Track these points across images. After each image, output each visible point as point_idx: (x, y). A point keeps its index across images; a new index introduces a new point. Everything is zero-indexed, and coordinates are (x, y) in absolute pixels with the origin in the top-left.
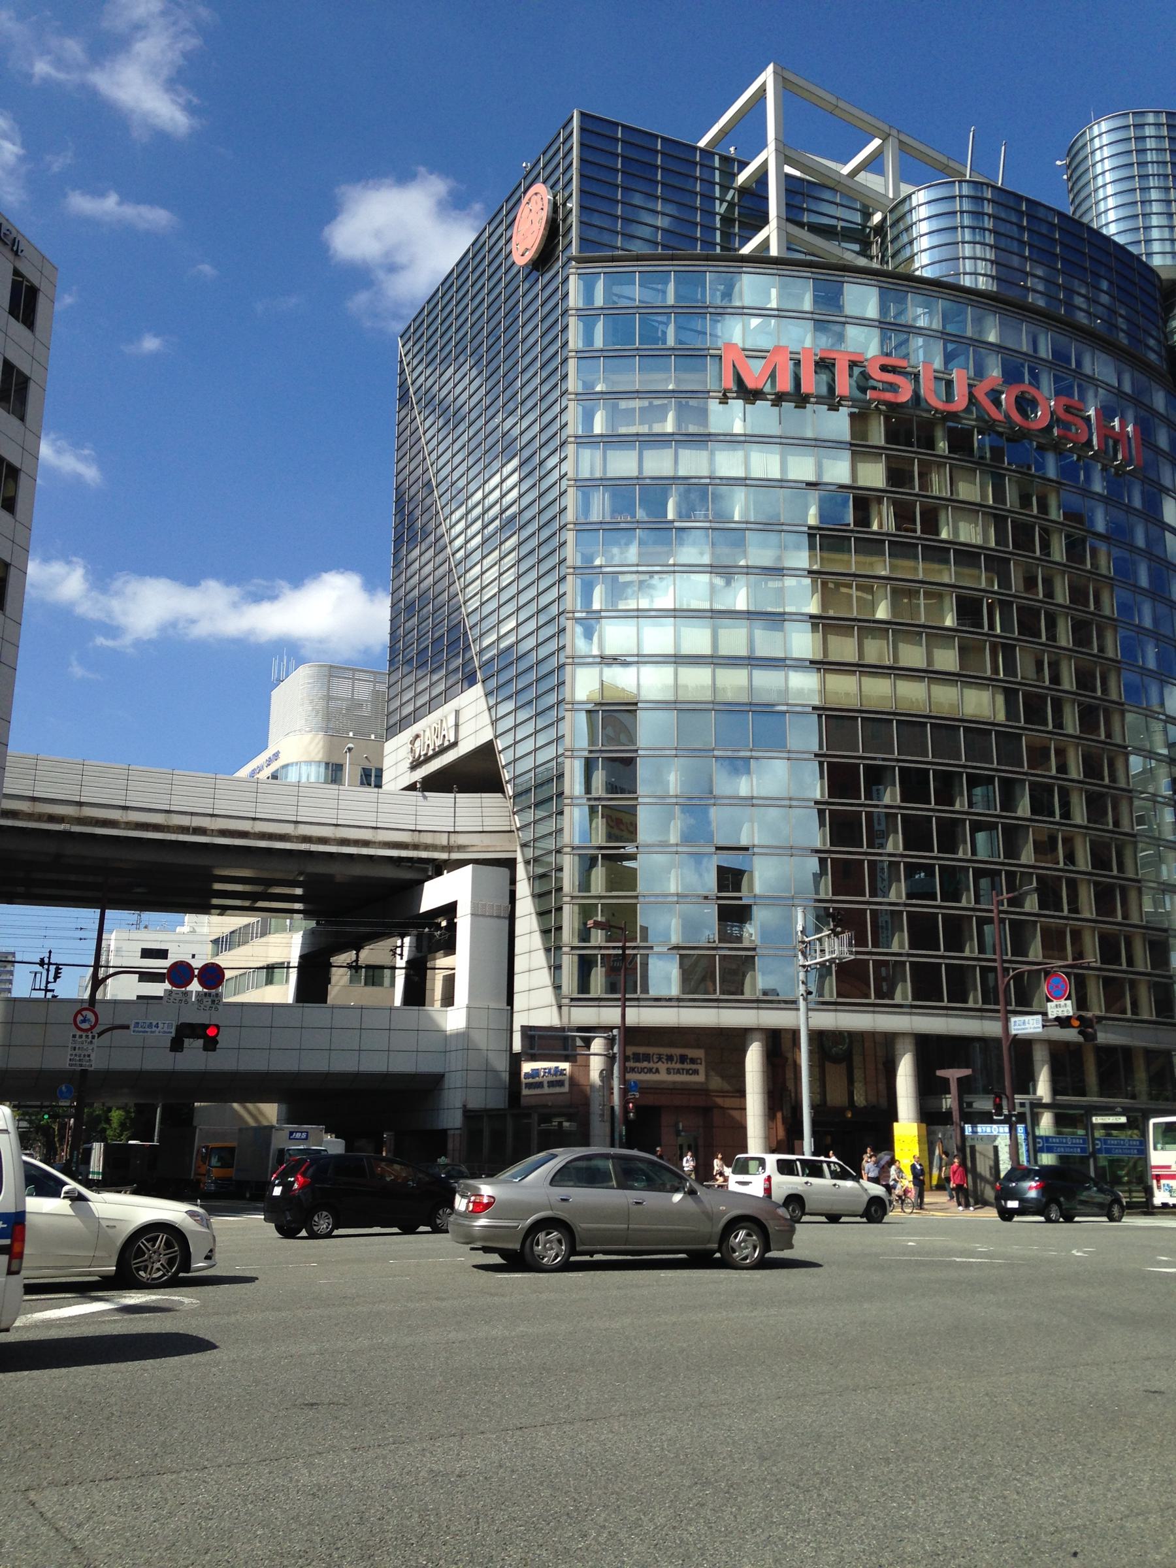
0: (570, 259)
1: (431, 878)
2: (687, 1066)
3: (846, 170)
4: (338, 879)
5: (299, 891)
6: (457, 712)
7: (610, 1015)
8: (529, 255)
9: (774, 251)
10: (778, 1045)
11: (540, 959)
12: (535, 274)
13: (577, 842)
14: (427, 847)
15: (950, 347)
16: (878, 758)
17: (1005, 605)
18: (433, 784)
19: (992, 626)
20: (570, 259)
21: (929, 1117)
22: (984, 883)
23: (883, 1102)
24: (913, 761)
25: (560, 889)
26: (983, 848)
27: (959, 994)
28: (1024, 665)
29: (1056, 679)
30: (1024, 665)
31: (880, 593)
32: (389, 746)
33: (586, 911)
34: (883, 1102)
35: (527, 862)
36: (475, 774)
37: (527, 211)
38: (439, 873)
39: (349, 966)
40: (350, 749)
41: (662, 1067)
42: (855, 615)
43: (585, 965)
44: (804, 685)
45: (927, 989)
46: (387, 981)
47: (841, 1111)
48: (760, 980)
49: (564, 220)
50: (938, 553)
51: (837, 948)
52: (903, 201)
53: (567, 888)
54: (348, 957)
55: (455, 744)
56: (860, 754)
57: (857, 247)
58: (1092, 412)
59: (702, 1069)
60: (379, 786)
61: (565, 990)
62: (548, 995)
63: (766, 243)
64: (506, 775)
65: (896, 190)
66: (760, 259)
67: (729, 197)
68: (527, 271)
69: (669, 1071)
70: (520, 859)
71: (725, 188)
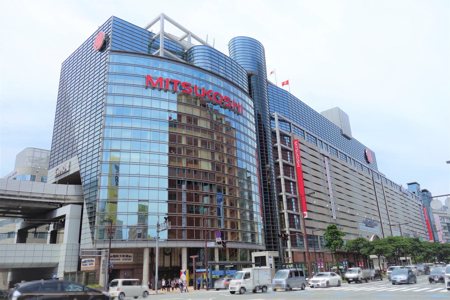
1: (59, 208)
2: (128, 258)
5: (19, 211)
6: (70, 163)
7: (107, 245)
9: (161, 55)
10: (152, 251)
11: (89, 230)
12: (99, 53)
14: (58, 199)
15: (201, 82)
17: (212, 143)
18: (62, 182)
19: (209, 148)
21: (190, 268)
23: (179, 265)
26: (206, 200)
27: (198, 237)
28: (217, 158)
29: (223, 161)
30: (217, 158)
32: (50, 171)
35: (87, 204)
36: (74, 179)
38: (61, 206)
39: (33, 233)
41: (121, 258)
46: (46, 237)
47: (168, 268)
49: (108, 41)
50: (198, 129)
52: (192, 48)
54: (34, 230)
55: (69, 171)
56: (177, 177)
57: (181, 57)
59: (132, 258)
61: (95, 238)
63: (159, 53)
64: (82, 180)
70: (85, 203)
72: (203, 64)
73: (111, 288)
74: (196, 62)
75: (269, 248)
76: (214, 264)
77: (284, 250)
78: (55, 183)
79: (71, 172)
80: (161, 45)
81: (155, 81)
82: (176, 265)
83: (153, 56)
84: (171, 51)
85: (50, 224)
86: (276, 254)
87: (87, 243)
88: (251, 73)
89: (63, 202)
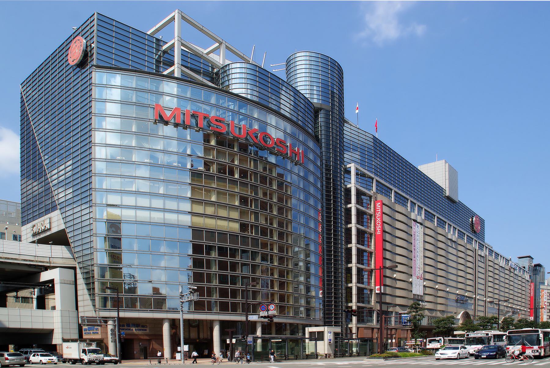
0: (92, 66)
3: (206, 52)
4: (7, 270)
6: (50, 219)
7: (114, 314)
8: (76, 62)
9: (176, 75)
10: (174, 324)
11: (87, 297)
12: (78, 69)
13: (99, 263)
15: (241, 117)
16: (211, 243)
17: (256, 200)
18: (44, 241)
19: (251, 206)
20: (92, 66)
22: (245, 280)
23: (209, 338)
24: (223, 245)
25: (94, 277)
27: (210, 309)
31: (213, 193)
33: (103, 284)
34: (209, 338)
35: (80, 268)
36: (59, 238)
37: (74, 46)
40: (7, 228)
42: (203, 199)
43: (105, 300)
44: (187, 220)
45: (224, 308)
46: (30, 302)
48: (169, 304)
49: (90, 51)
51: (195, 297)
52: (226, 66)
53: (96, 276)
54: (14, 294)
55: (50, 229)
56: (204, 242)
57: (209, 79)
58: (288, 144)
59: (148, 329)
60: (20, 241)
61: (97, 306)
62: (91, 307)
63: (173, 72)
64: (71, 241)
65: (224, 61)
66: (170, 77)
67: (159, 54)
68: (74, 67)
69: (136, 330)
70: (78, 267)
71: (158, 50)
72: (244, 91)
73: (144, 290)
74: (234, 86)
75: (327, 323)
76: (256, 337)
77: (347, 325)
78: (33, 242)
79: (54, 230)
80: (177, 59)
81: (168, 114)
82: (205, 336)
83: (164, 76)
84: (191, 69)
85: (34, 289)
86: (338, 330)
87: (87, 309)
88: (320, 107)
89: (48, 265)
